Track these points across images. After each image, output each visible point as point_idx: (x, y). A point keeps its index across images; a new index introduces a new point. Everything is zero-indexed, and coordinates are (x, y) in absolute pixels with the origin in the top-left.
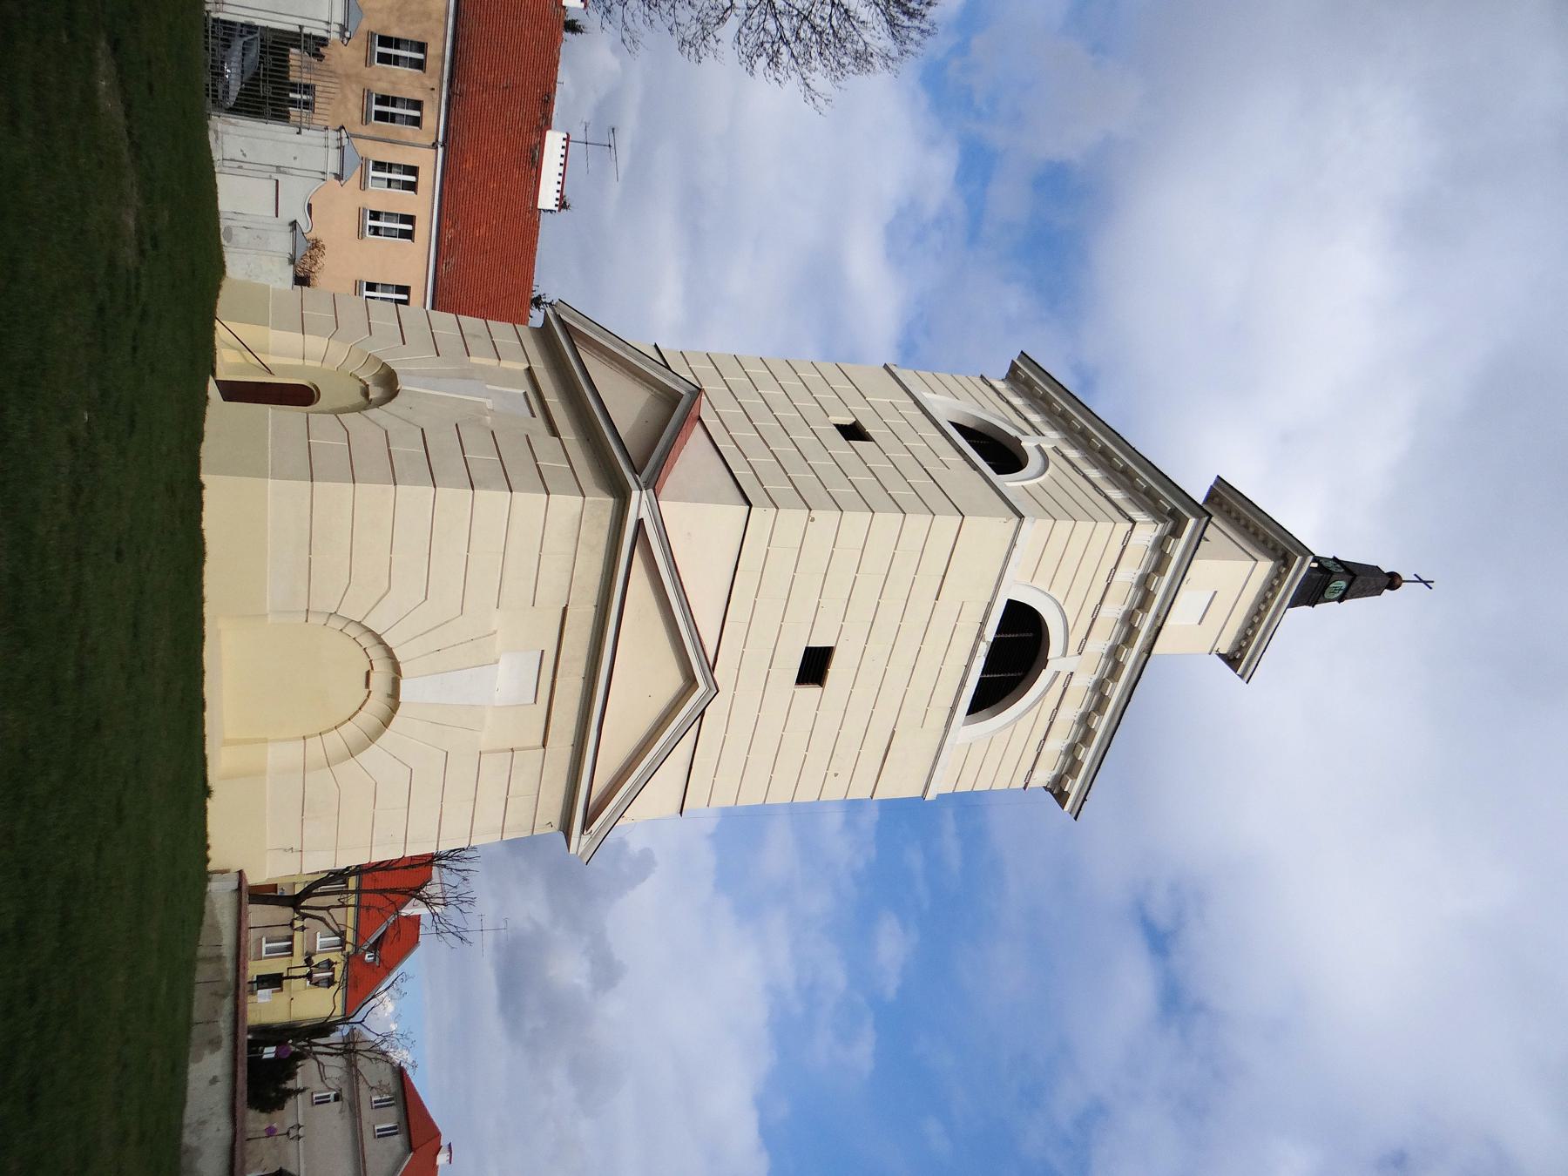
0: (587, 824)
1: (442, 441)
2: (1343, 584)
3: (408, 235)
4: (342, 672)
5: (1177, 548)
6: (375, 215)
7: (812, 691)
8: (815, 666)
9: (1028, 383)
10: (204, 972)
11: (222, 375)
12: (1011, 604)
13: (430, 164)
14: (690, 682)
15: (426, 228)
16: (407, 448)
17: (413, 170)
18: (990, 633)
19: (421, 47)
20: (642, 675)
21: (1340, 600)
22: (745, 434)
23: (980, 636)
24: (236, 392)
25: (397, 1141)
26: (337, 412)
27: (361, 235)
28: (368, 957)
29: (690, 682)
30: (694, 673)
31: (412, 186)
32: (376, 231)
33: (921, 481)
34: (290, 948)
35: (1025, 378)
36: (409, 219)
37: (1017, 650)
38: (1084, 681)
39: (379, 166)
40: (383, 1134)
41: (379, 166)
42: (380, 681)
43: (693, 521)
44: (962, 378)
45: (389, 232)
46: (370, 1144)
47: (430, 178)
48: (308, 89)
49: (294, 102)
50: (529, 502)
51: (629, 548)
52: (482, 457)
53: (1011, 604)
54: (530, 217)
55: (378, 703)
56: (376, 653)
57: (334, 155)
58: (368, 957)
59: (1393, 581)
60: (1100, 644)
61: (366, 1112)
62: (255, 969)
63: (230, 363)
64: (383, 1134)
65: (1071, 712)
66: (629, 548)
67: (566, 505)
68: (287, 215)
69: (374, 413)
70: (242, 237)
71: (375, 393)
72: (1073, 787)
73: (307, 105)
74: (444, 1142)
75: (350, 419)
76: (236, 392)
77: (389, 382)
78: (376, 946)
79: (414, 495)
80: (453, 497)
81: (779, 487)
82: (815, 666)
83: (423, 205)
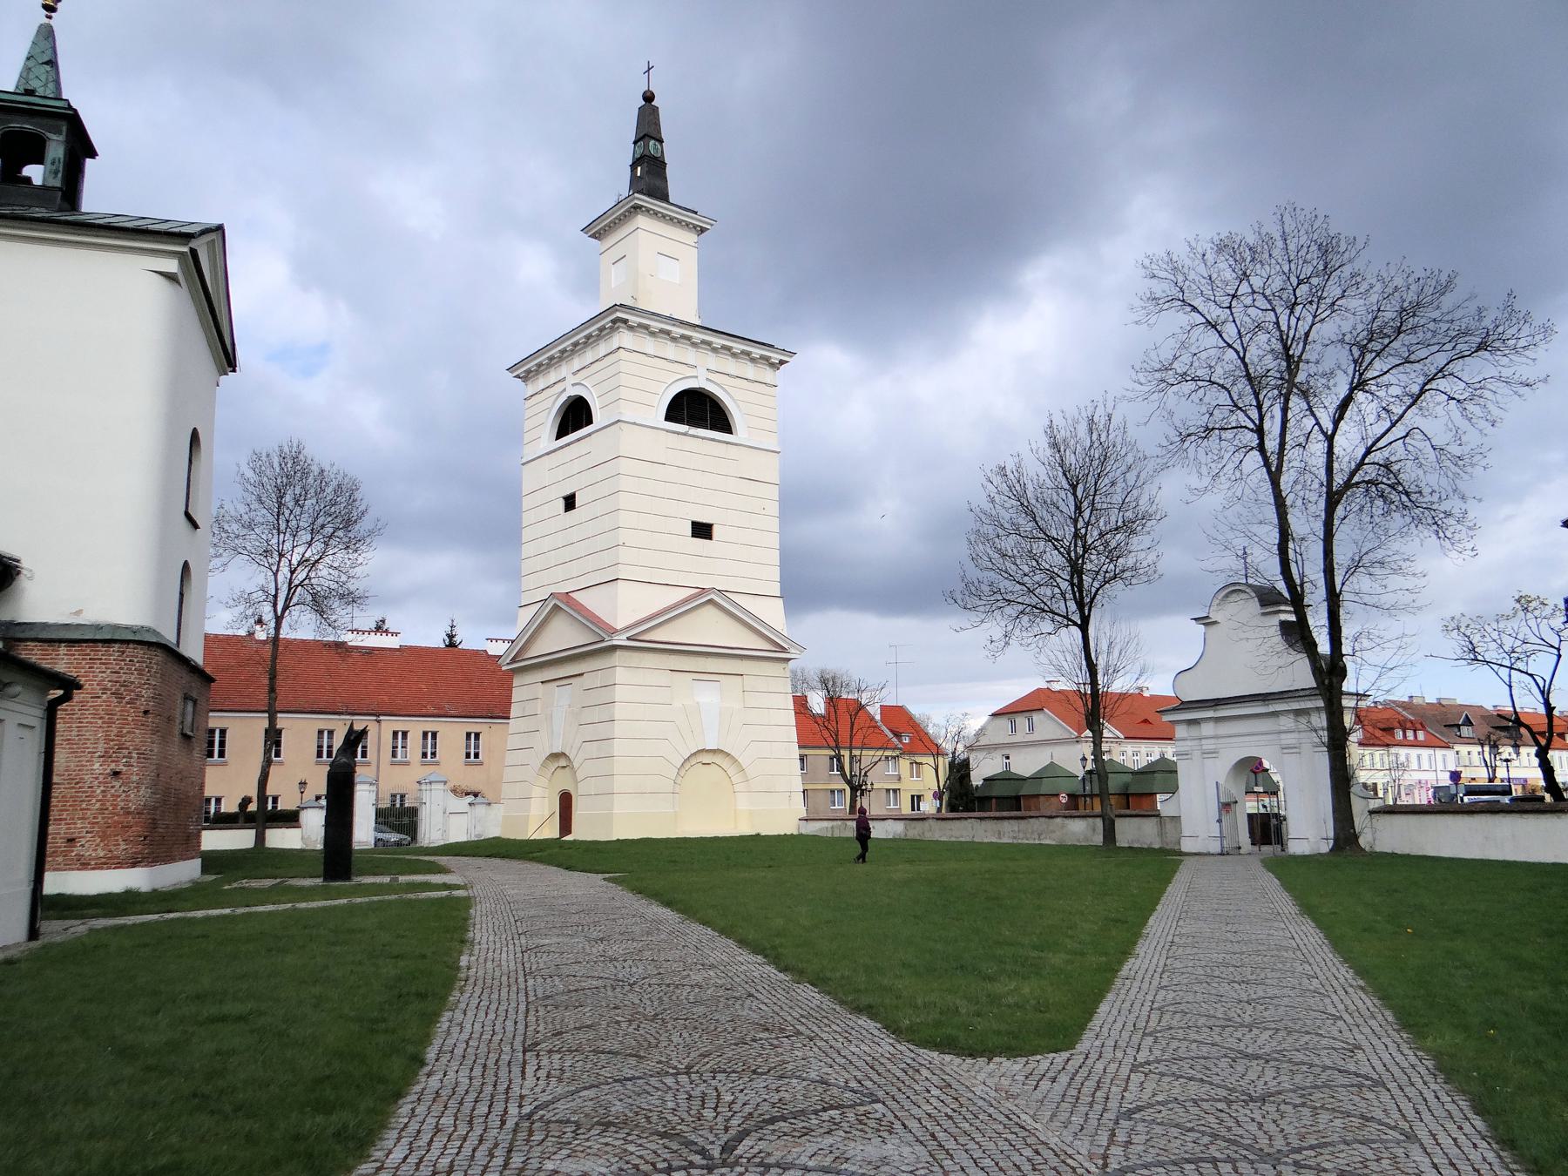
0: (784, 650)
1: (589, 733)
2: (652, 142)
3: (434, 735)
4: (703, 777)
5: (634, 319)
6: (424, 755)
7: (716, 531)
8: (702, 530)
9: (528, 372)
10: (837, 834)
11: (556, 835)
12: (668, 418)
13: (390, 724)
14: (711, 601)
15: (430, 725)
16: (592, 749)
17: (395, 734)
18: (683, 428)
19: (321, 732)
20: (708, 629)
21: (661, 141)
22: (575, 568)
23: (685, 434)
24: (566, 826)
25: (1036, 717)
26: (576, 782)
27: (437, 764)
28: (906, 741)
29: (711, 601)
30: (705, 599)
31: (405, 734)
32: (434, 754)
33: (599, 474)
34: (895, 791)
35: (529, 370)
36: (425, 734)
37: (697, 409)
38: (713, 361)
39: (394, 755)
40: (1031, 728)
41: (394, 755)
42: (706, 758)
43: (624, 608)
44: (528, 413)
45: (434, 746)
46: (1035, 737)
47: (399, 724)
48: (394, 796)
49: (275, 807)
50: (619, 693)
51: (641, 644)
52: (595, 715)
53: (668, 418)
54: (402, 649)
55: (718, 759)
56: (693, 761)
57: (434, 786)
58: (906, 741)
59: (649, 97)
60: (690, 355)
61: (1018, 738)
62: (906, 810)
63: (551, 831)
64: (1031, 728)
65: (731, 366)
66: (641, 644)
67: (621, 675)
68: (466, 808)
69: (576, 765)
70: (479, 830)
71: (563, 763)
72: (776, 357)
73: (402, 796)
74: (1045, 686)
75: (580, 776)
76: (566, 826)
77: (555, 756)
78: (897, 735)
79: (618, 747)
80: (618, 729)
81: (606, 559)
82: (702, 530)
83: (416, 727)
